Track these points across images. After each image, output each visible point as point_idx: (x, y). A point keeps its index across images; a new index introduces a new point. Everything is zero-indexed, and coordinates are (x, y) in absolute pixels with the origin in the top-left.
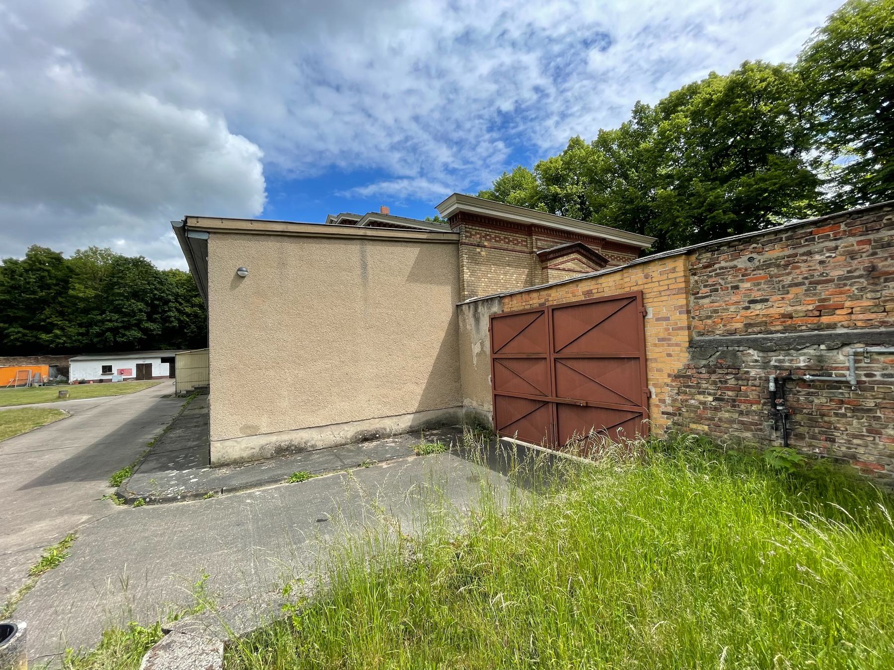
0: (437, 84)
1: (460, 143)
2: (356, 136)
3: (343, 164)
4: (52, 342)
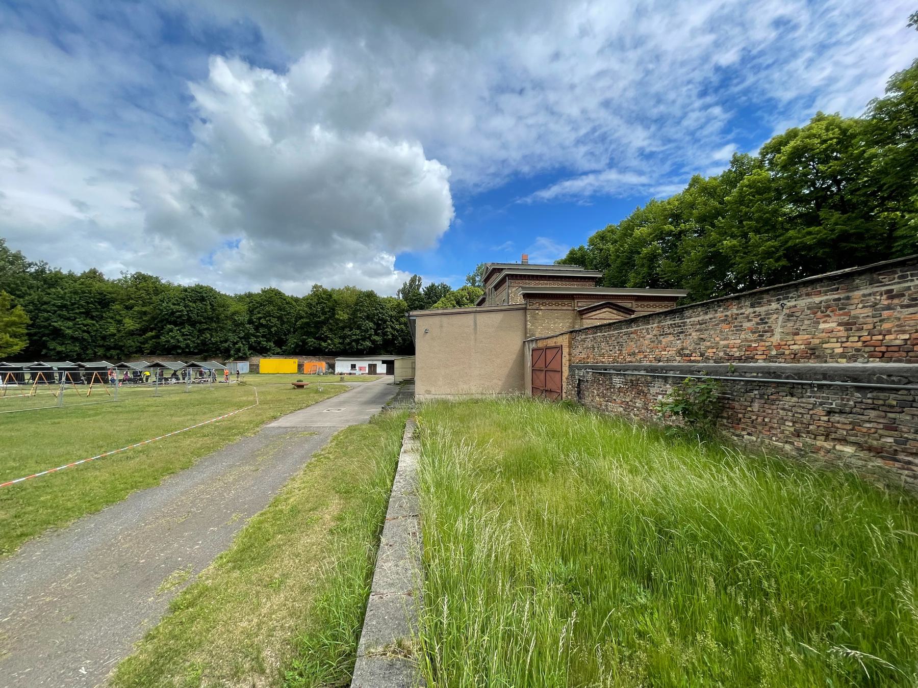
0: (633, 55)
1: (661, 121)
2: (540, 137)
3: (526, 169)
4: (327, 348)
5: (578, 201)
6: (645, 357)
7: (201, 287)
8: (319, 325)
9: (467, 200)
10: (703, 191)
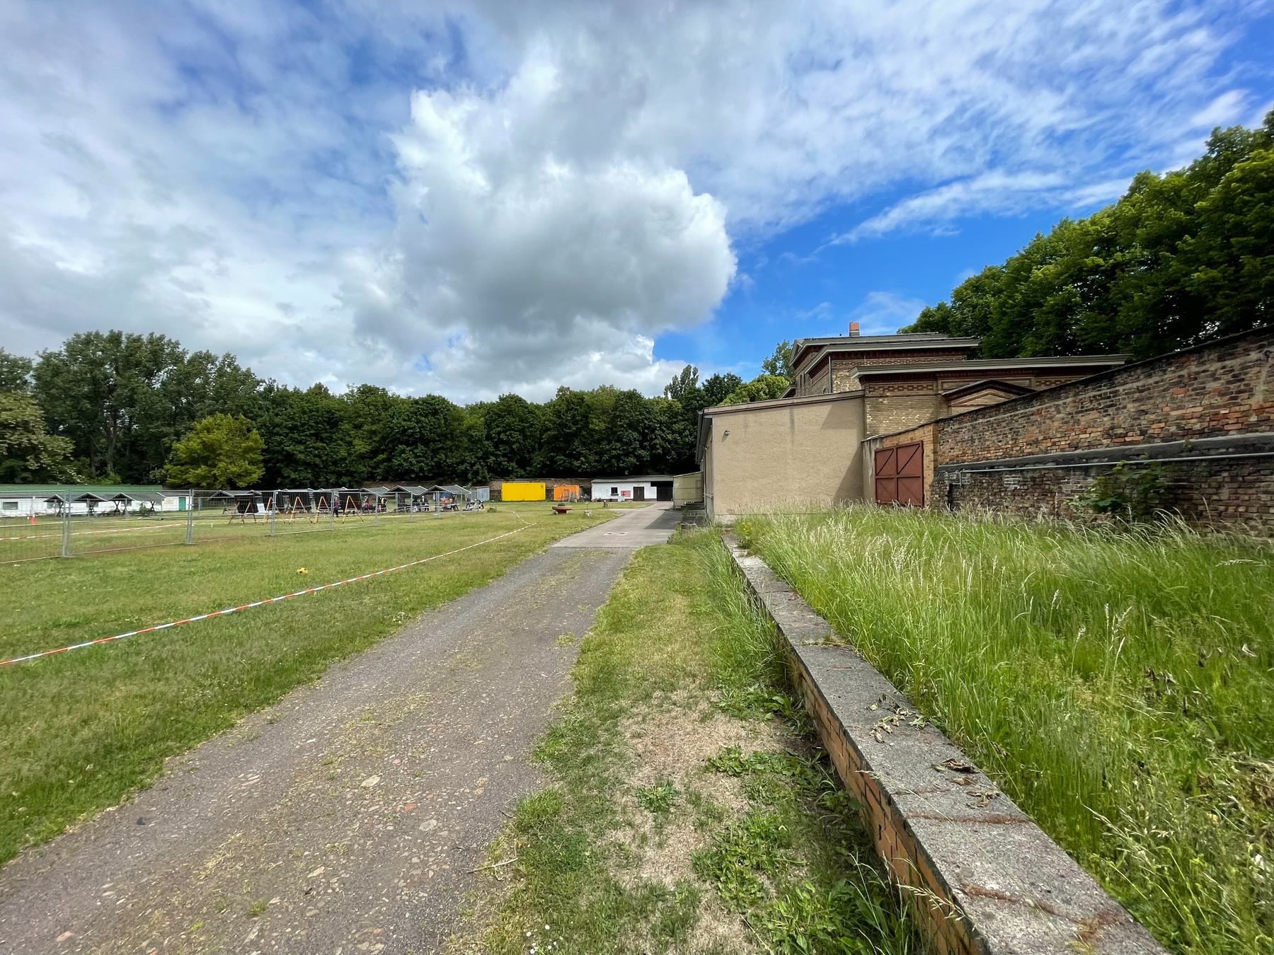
1: (1087, 73)
2: (869, 135)
5: (932, 230)
6: (1054, 444)
7: (434, 398)
8: (569, 438)
9: (752, 247)
10: (1155, 197)
